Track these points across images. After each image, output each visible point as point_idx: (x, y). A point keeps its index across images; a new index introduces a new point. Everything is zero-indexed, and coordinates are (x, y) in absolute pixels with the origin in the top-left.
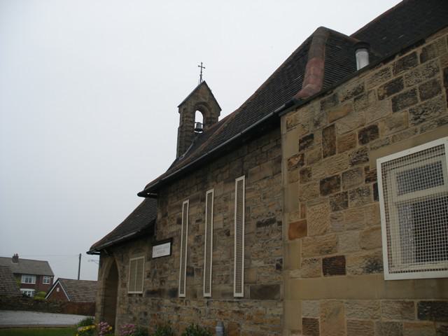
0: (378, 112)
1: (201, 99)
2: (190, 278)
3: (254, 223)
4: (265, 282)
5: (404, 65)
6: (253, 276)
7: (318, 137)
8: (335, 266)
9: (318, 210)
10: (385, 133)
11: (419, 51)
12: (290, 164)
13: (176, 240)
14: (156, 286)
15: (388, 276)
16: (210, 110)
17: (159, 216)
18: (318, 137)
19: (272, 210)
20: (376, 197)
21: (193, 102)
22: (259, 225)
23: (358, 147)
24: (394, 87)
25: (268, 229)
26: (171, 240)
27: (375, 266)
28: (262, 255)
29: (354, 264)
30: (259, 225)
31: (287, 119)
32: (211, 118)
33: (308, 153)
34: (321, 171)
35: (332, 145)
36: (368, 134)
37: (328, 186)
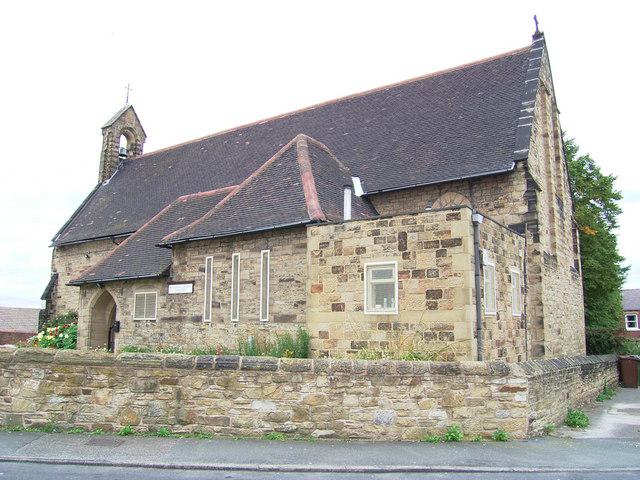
0: (368, 242)
1: (125, 125)
2: (216, 309)
3: (276, 281)
4: (285, 313)
5: (381, 224)
6: (276, 309)
7: (332, 244)
8: (337, 307)
9: (330, 281)
10: (369, 252)
11: (389, 220)
12: (313, 254)
13: (199, 283)
14: (175, 313)
15: (366, 313)
16: (136, 136)
17: (176, 263)
18: (332, 244)
19: (292, 274)
20: (363, 279)
21: (120, 127)
22: (281, 281)
23: (355, 255)
24: (376, 233)
25: (288, 284)
26: (193, 282)
27: (360, 309)
28: (526, 339)
29: (350, 306)
30: (281, 281)
31: (311, 229)
32: (136, 145)
33: (325, 251)
34: (333, 261)
35: (340, 250)
36: (361, 250)
37: (336, 270)
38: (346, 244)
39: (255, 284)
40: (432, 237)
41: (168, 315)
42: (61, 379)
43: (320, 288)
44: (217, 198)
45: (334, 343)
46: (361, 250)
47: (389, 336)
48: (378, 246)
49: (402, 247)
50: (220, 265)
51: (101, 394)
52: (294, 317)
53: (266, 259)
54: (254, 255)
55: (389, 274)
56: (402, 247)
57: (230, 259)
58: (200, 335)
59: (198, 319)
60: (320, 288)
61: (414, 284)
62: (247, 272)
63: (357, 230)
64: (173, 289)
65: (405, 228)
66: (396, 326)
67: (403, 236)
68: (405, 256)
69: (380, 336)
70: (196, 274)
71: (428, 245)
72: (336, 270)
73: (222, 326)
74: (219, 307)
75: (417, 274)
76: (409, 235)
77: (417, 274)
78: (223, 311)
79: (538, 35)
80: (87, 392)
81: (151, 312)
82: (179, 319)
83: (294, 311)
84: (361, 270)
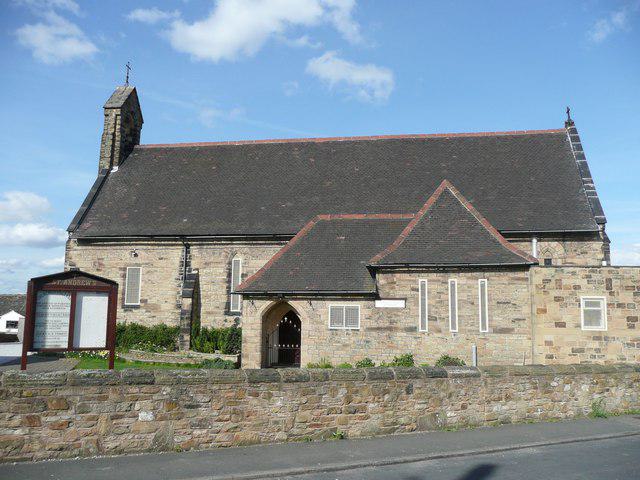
3: (494, 303)
7: (553, 281)
8: (561, 325)
9: (552, 307)
10: (584, 289)
18: (553, 281)
26: (405, 299)
33: (547, 285)
34: (554, 293)
37: (557, 299)
38: (565, 282)
39: (473, 304)
40: (630, 284)
41: (375, 325)
42: (597, 383)
43: (545, 311)
44: (402, 224)
45: (558, 349)
46: (577, 287)
47: (601, 344)
48: (590, 286)
49: (609, 287)
50: (437, 287)
51: (613, 390)
52: (513, 329)
53: (483, 286)
54: (470, 282)
55: (597, 304)
56: (609, 287)
57: (447, 283)
58: (414, 342)
59: (412, 330)
60: (545, 311)
61: (619, 312)
62: (465, 294)
63: (574, 273)
64: (379, 304)
65: (611, 276)
66: (606, 339)
67: (609, 281)
68: (611, 294)
69: (596, 345)
70: (408, 293)
71: (627, 288)
72: (557, 299)
73: (440, 335)
74: (436, 319)
75: (620, 305)
76: (614, 281)
77: (620, 305)
78: (439, 324)
79: (569, 123)
80: (608, 390)
81: (355, 322)
82: (389, 329)
83: (511, 326)
84: (578, 301)
